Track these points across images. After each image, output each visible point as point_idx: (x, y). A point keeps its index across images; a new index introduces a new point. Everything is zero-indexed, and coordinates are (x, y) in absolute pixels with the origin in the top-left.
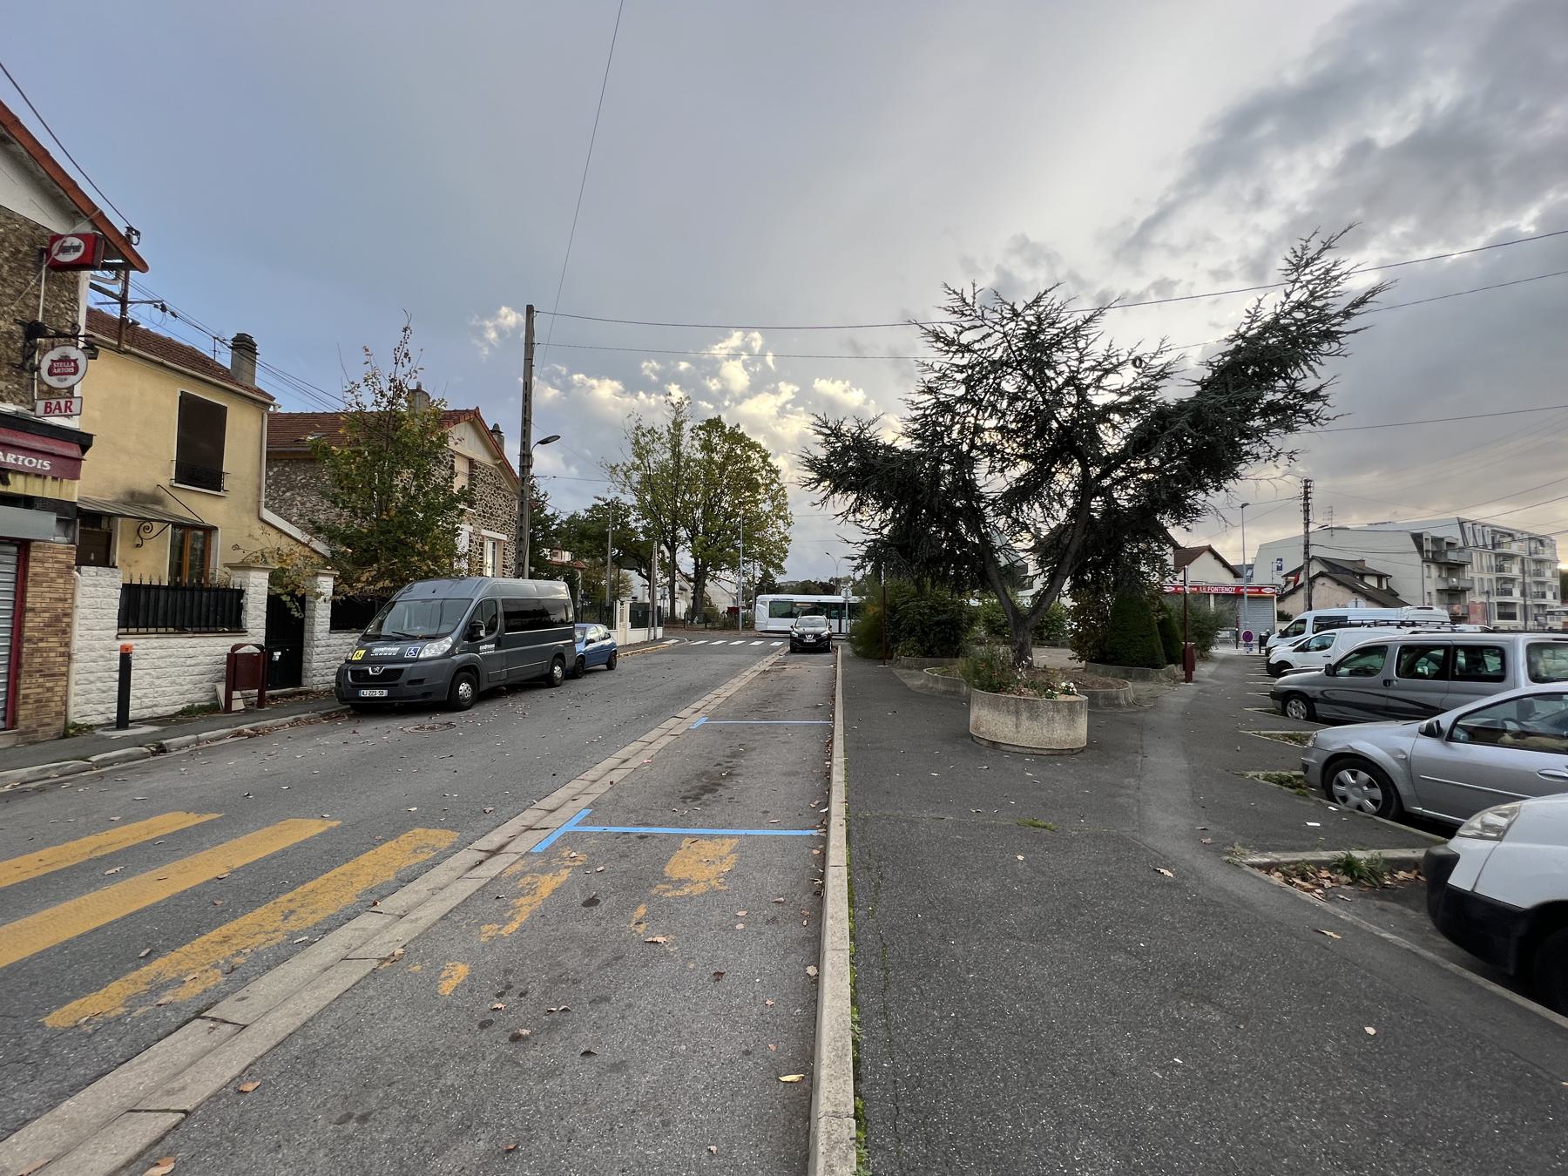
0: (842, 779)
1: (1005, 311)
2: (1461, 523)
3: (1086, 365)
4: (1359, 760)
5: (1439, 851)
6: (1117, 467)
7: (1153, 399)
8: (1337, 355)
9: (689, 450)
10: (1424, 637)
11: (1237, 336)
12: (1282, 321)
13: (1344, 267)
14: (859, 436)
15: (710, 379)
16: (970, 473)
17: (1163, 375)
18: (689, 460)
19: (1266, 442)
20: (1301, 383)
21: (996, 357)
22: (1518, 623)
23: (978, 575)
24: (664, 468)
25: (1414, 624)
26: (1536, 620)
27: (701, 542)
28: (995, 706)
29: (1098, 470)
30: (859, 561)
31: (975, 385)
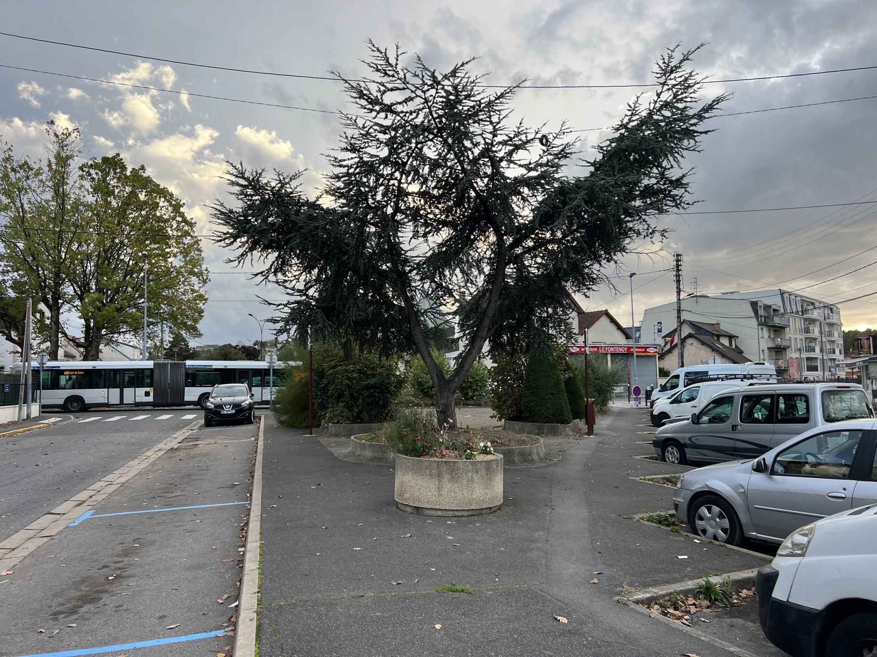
0: (255, 566)
1: (426, 77)
2: (782, 293)
3: (499, 139)
4: (712, 497)
5: (767, 570)
6: (527, 237)
7: (557, 176)
8: (693, 150)
9: (77, 192)
10: (759, 388)
11: (621, 126)
12: (655, 117)
13: (698, 78)
14: (279, 190)
15: (109, 112)
16: (395, 236)
17: (563, 154)
18: (77, 204)
19: (644, 220)
20: (669, 171)
21: (418, 121)
22: (819, 373)
23: (405, 338)
24: (41, 209)
25: (752, 377)
26: (830, 371)
27: (94, 301)
28: (417, 471)
29: (511, 239)
30: (282, 324)
31: (397, 148)
